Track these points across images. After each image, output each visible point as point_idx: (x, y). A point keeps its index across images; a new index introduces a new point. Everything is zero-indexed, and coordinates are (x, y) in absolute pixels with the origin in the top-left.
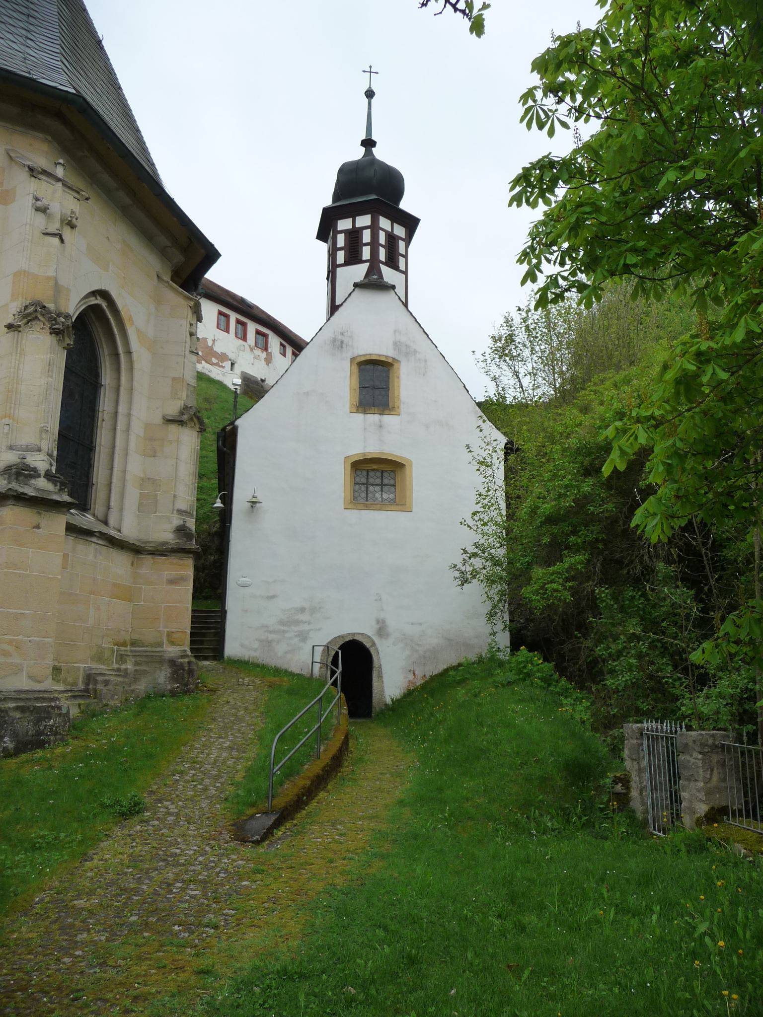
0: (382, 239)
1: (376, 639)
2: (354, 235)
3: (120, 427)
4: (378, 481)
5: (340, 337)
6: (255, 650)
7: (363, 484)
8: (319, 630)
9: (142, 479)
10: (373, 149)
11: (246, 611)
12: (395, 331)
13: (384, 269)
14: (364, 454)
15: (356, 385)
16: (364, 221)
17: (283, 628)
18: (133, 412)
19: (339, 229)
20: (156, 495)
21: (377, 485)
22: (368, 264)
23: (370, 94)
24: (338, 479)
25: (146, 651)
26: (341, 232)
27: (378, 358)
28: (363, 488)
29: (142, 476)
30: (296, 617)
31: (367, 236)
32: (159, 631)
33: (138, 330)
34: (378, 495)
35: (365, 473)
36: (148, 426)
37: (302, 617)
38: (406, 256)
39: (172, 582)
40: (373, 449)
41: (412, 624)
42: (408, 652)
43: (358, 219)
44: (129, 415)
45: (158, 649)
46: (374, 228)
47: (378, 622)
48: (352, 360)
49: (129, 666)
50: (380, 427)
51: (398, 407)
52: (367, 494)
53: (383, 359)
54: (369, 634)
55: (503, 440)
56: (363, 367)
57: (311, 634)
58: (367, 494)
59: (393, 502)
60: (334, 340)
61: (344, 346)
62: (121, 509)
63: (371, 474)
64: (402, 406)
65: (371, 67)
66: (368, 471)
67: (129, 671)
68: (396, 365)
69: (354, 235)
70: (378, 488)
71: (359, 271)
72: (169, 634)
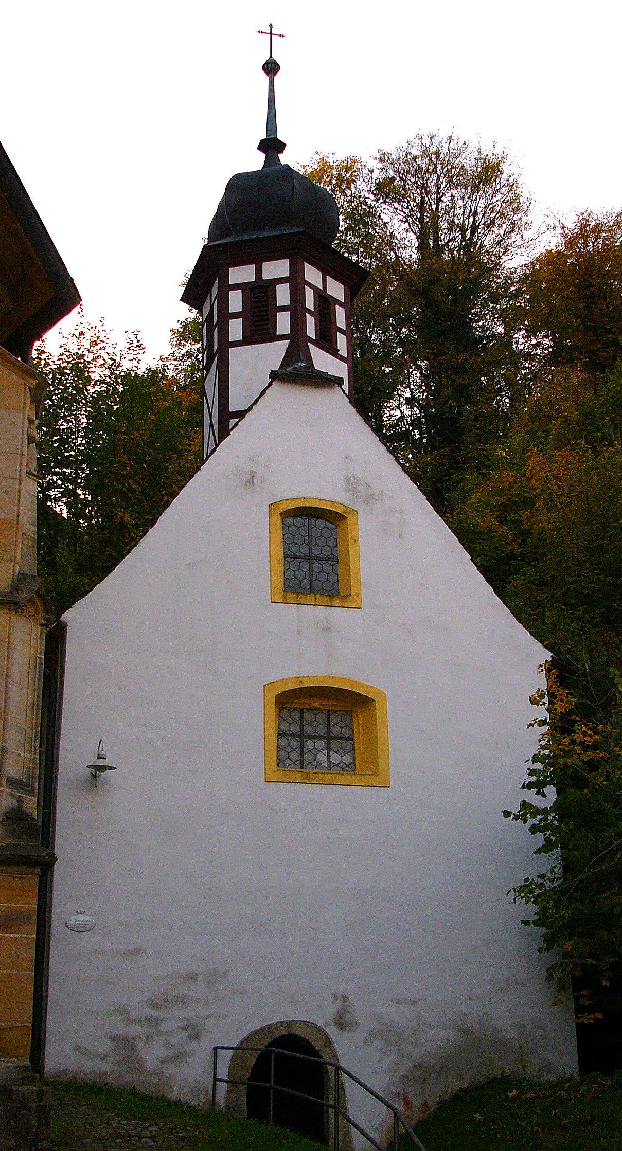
0: (310, 303)
1: (333, 1033)
2: (259, 295)
4: (322, 730)
5: (249, 467)
6: (104, 1057)
7: (294, 735)
8: (225, 1015)
13: (314, 350)
16: (278, 269)
21: (320, 738)
23: (271, 68)
26: (236, 287)
28: (294, 743)
30: (180, 992)
31: (283, 295)
34: (322, 757)
35: (296, 715)
40: (316, 670)
41: (398, 1002)
42: (391, 1059)
43: (266, 266)
46: (296, 282)
50: (328, 629)
51: (358, 595)
56: (289, 521)
59: (350, 768)
63: (308, 717)
64: (364, 592)
65: (271, 26)
68: (350, 518)
69: (259, 295)
70: (321, 744)
71: (273, 354)
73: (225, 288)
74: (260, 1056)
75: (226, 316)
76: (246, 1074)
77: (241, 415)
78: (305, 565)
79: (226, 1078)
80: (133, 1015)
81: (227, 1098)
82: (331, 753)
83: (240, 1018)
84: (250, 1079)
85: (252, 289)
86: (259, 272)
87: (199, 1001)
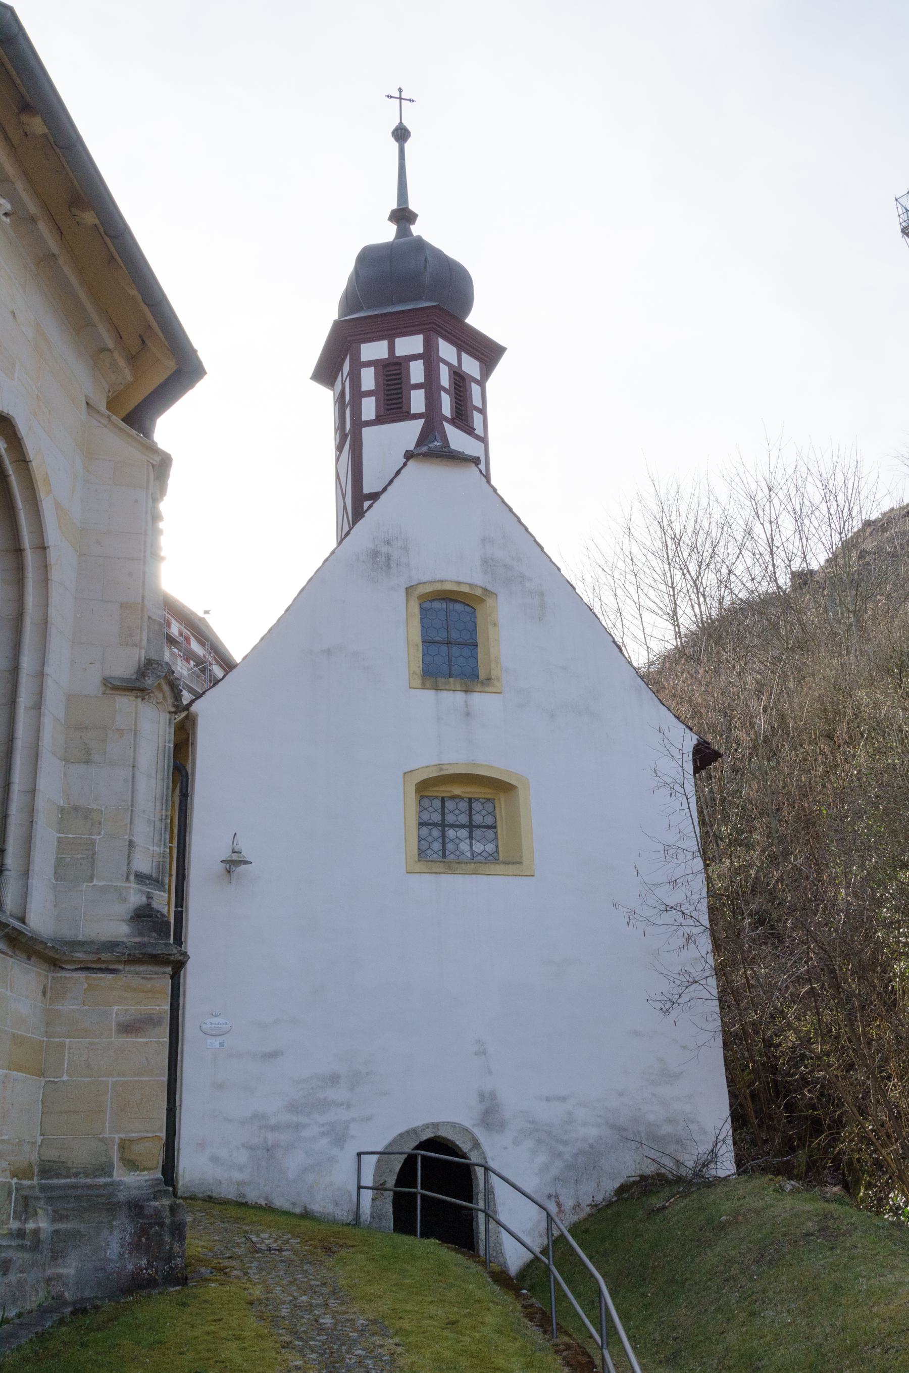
0: (445, 379)
2: (393, 373)
3: (24, 699)
4: (464, 819)
5: (384, 549)
6: (241, 1169)
7: (435, 825)
8: (369, 1119)
9: (62, 810)
10: (412, 227)
11: (220, 1087)
12: (484, 540)
13: (450, 429)
14: (440, 766)
15: (416, 636)
17: (295, 1119)
18: (48, 670)
19: (364, 358)
20: (92, 843)
21: (462, 826)
22: (421, 422)
23: (401, 134)
24: (394, 819)
25: (74, 1187)
26: (368, 364)
28: (436, 833)
29: (61, 803)
31: (417, 372)
32: (103, 1140)
33: (57, 505)
34: (464, 846)
36: (72, 700)
37: (332, 1094)
38: (483, 411)
39: (129, 1028)
40: (457, 758)
41: (548, 1099)
42: (542, 1159)
44: (41, 675)
45: (102, 1180)
46: (430, 357)
47: (482, 1097)
48: (409, 590)
49: (42, 1223)
50: (468, 714)
51: (498, 679)
52: (444, 844)
53: (466, 589)
54: (467, 1124)
55: (691, 741)
56: (427, 605)
58: (444, 844)
59: (493, 858)
60: (375, 554)
61: (393, 565)
62: (26, 873)
63: (450, 805)
65: (400, 90)
66: (443, 800)
67: (42, 1236)
68: (490, 602)
69: (393, 373)
70: (463, 833)
71: (407, 433)
72: (124, 1146)
73: (358, 365)
74: (406, 1160)
76: (391, 1181)
77: (374, 497)
78: (444, 648)
79: (370, 1184)
80: (273, 1121)
81: (372, 1207)
82: (474, 842)
84: (396, 1186)
85: (384, 366)
87: (342, 1104)
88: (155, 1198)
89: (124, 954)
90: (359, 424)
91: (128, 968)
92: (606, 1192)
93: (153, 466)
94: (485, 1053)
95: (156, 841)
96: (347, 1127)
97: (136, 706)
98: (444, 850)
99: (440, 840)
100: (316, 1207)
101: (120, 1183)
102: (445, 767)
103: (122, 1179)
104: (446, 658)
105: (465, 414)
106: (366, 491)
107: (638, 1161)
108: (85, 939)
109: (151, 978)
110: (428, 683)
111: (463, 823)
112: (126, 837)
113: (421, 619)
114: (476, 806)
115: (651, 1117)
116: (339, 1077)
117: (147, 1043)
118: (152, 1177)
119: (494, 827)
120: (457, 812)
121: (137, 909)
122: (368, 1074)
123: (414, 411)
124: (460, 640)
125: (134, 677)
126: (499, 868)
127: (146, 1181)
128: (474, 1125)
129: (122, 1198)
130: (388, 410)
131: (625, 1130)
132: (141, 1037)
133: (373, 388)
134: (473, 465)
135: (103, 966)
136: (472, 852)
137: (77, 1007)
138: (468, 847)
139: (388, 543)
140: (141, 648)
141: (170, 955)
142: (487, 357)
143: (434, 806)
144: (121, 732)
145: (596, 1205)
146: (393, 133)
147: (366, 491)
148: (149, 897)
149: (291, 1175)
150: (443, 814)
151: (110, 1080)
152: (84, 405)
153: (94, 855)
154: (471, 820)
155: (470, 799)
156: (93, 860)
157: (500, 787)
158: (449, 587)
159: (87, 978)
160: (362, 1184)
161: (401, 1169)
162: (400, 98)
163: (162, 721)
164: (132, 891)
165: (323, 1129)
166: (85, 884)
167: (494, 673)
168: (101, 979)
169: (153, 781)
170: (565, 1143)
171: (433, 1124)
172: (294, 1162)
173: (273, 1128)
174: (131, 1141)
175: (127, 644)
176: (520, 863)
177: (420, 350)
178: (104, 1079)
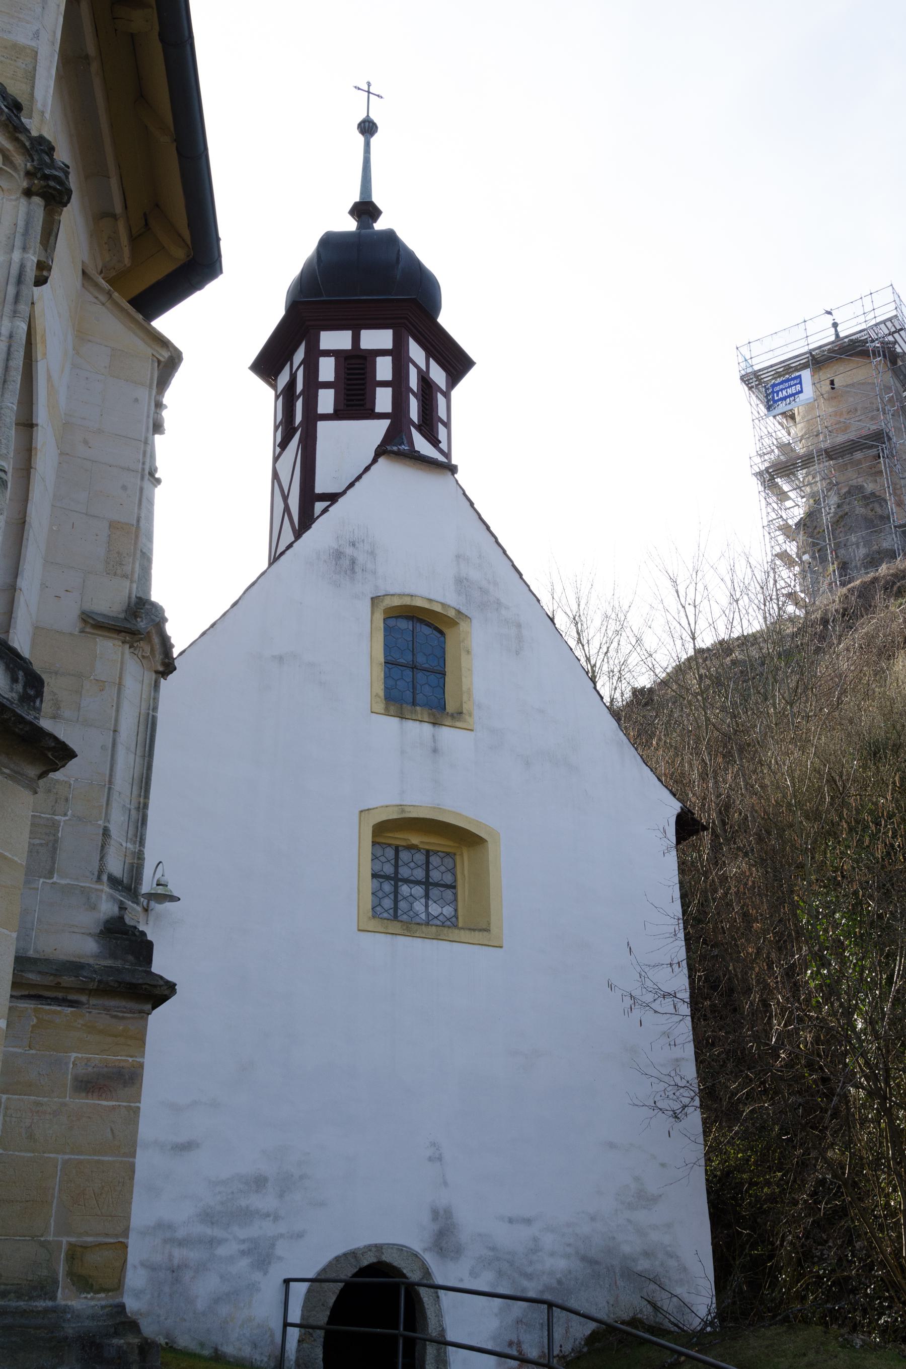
1: (429, 1259)
2: (356, 370)
4: (420, 874)
5: (349, 551)
8: (300, 1235)
12: (458, 557)
16: (377, 339)
17: (209, 1231)
19: (323, 346)
20: (55, 825)
21: (418, 883)
22: (386, 423)
23: (368, 128)
24: (346, 867)
26: (327, 353)
27: (426, 605)
28: (435, 875)
30: (243, 1203)
31: (384, 369)
32: (43, 1245)
34: (419, 906)
35: (390, 853)
38: (447, 425)
40: (421, 801)
41: (511, 1221)
45: (41, 1304)
46: (399, 355)
47: (435, 1214)
48: (375, 601)
50: (435, 751)
51: (470, 715)
52: (396, 901)
53: (438, 608)
54: (417, 1247)
56: (392, 622)
57: (281, 1249)
58: (396, 901)
59: (452, 923)
60: (338, 555)
61: (357, 569)
63: (404, 856)
65: (369, 84)
66: (397, 849)
68: (463, 626)
69: (356, 370)
70: (418, 891)
72: (75, 1254)
73: (314, 355)
74: (342, 1291)
75: (313, 384)
76: (322, 1317)
77: (333, 498)
78: (408, 673)
79: (298, 1321)
80: (181, 1233)
81: (298, 1351)
82: (430, 902)
83: (317, 1245)
84: (328, 1323)
85: (346, 358)
86: (356, 340)
87: (268, 1215)
88: (116, 1334)
89: (93, 980)
90: (312, 417)
91: (93, 1001)
92: (575, 1340)
93: (159, 362)
94: (440, 1159)
95: (130, 835)
96: (273, 1246)
97: (123, 654)
98: (396, 908)
99: (392, 896)
100: (229, 1350)
101: (66, 1309)
102: (407, 809)
103: (69, 1303)
104: (411, 685)
105: (431, 424)
106: (319, 489)
107: (611, 1303)
108: (37, 956)
109: (123, 1018)
110: (392, 709)
111: (419, 878)
112: (100, 822)
113: (385, 636)
114: (435, 860)
115: (626, 1249)
116: (266, 1180)
117: (114, 1108)
118: (111, 1302)
119: (453, 887)
120: (412, 865)
121: (107, 922)
122: (301, 1177)
123: (379, 409)
124: (426, 666)
125: (122, 616)
126: (464, 935)
127: (103, 1307)
128: (425, 1250)
129: (71, 1331)
130: (348, 406)
131: (597, 1263)
132: (106, 1099)
133: (332, 379)
134: (450, 473)
135: (60, 995)
136: (428, 914)
137: (20, 1050)
138: (424, 908)
139: (354, 545)
140: (132, 582)
141: (155, 986)
142: (456, 370)
143: (387, 855)
144: (101, 685)
145: (564, 1357)
146: (359, 125)
147: (319, 489)
148: (122, 908)
149: (200, 1305)
150: (396, 866)
151: (60, 1157)
152: (80, 272)
153: (56, 841)
154: (396, 887)
155: (428, 851)
156: (55, 849)
157: (465, 839)
158: (419, 603)
159: (35, 1010)
160: (290, 1320)
161: (335, 1302)
162: (369, 92)
163: (146, 682)
164: (104, 897)
165: (243, 1247)
166: (42, 880)
167: (465, 707)
168: (55, 1012)
169: (132, 756)
170: (529, 1277)
171: (376, 1246)
172: (204, 1288)
173: (182, 1243)
174: (85, 1247)
175: (115, 574)
176: (487, 930)
177: (389, 345)
178: (52, 1155)
